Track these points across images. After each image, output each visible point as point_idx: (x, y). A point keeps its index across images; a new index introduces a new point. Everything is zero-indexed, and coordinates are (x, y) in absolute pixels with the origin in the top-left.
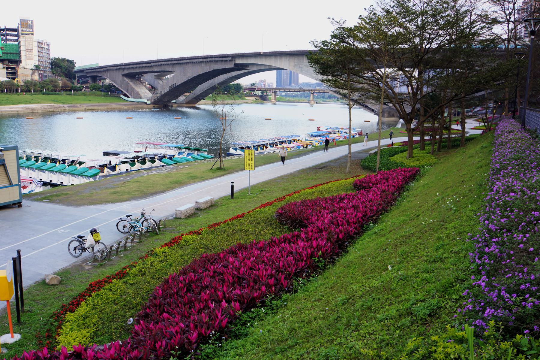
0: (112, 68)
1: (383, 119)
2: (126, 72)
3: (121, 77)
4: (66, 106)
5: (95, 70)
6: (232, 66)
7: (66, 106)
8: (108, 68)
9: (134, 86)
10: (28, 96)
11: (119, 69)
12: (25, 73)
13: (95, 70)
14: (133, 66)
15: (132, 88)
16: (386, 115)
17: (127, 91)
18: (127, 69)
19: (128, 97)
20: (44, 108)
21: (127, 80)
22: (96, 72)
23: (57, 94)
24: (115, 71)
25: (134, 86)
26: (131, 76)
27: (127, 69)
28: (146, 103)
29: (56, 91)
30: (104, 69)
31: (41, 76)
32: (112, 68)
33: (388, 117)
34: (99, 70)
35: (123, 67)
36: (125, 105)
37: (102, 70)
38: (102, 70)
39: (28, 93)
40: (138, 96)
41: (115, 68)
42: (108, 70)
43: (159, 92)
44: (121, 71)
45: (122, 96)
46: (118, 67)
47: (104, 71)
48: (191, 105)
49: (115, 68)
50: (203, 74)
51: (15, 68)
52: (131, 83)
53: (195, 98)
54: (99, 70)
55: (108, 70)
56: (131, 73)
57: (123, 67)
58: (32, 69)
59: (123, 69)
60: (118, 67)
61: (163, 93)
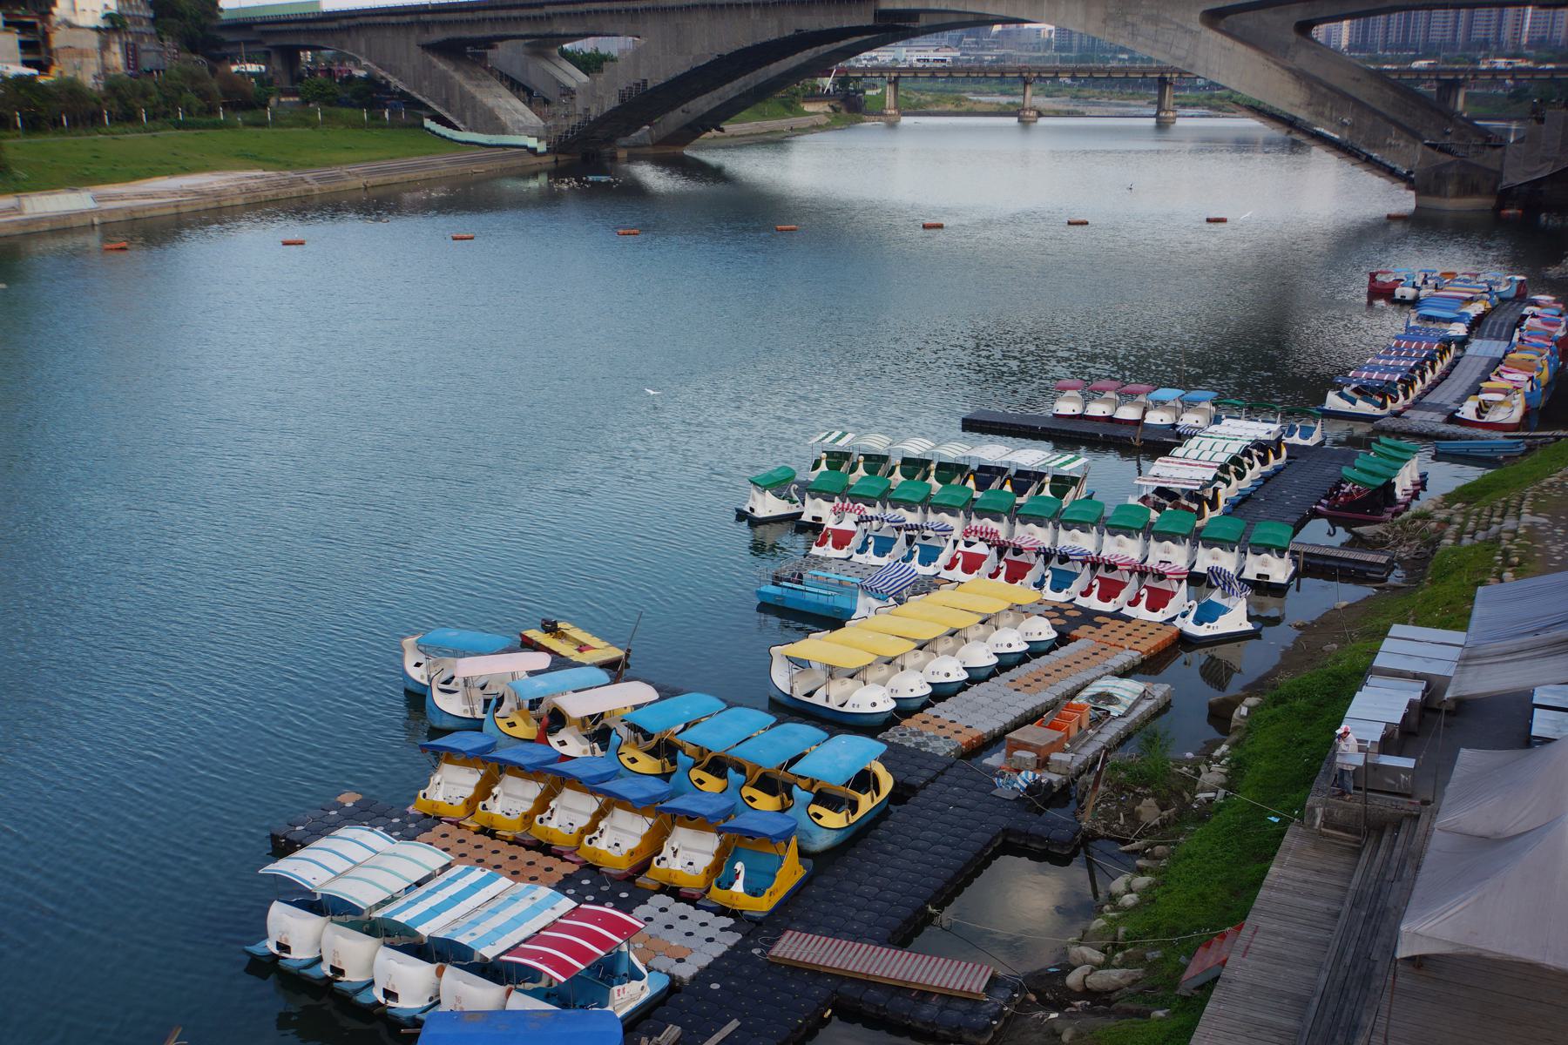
0: (379, 19)
1: (1433, 202)
2: (438, 35)
3: (416, 54)
4: (308, 177)
5: (303, 26)
6: (868, 21)
7: (308, 177)
8: (362, 20)
9: (469, 87)
10: (133, 141)
11: (410, 24)
12: (78, 44)
13: (303, 26)
14: (469, 16)
15: (464, 96)
16: (1451, 188)
17: (447, 105)
18: (443, 24)
19: (455, 128)
20: (249, 190)
21: (442, 65)
22: (309, 31)
23: (217, 126)
24: (389, 33)
25: (469, 87)
26: (452, 50)
27: (443, 24)
28: (533, 151)
29: (212, 111)
30: (345, 22)
31: (131, 53)
32: (379, 19)
33: (1457, 195)
34: (320, 25)
35: (428, 17)
36: (473, 161)
37: (335, 25)
38: (335, 25)
39: (129, 126)
40: (492, 123)
41: (393, 20)
42: (359, 27)
43: (579, 109)
44: (417, 31)
45: (428, 123)
46: (408, 19)
47: (341, 30)
48: (671, 150)
49: (393, 20)
50: (756, 47)
51: (33, 25)
52: (458, 77)
53: (689, 126)
54: (320, 25)
55: (359, 27)
56: (454, 40)
57: (428, 17)
58: (97, 29)
59: (426, 26)
60: (408, 19)
61: (594, 112)
